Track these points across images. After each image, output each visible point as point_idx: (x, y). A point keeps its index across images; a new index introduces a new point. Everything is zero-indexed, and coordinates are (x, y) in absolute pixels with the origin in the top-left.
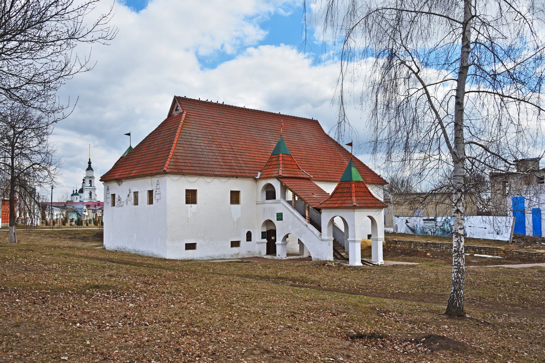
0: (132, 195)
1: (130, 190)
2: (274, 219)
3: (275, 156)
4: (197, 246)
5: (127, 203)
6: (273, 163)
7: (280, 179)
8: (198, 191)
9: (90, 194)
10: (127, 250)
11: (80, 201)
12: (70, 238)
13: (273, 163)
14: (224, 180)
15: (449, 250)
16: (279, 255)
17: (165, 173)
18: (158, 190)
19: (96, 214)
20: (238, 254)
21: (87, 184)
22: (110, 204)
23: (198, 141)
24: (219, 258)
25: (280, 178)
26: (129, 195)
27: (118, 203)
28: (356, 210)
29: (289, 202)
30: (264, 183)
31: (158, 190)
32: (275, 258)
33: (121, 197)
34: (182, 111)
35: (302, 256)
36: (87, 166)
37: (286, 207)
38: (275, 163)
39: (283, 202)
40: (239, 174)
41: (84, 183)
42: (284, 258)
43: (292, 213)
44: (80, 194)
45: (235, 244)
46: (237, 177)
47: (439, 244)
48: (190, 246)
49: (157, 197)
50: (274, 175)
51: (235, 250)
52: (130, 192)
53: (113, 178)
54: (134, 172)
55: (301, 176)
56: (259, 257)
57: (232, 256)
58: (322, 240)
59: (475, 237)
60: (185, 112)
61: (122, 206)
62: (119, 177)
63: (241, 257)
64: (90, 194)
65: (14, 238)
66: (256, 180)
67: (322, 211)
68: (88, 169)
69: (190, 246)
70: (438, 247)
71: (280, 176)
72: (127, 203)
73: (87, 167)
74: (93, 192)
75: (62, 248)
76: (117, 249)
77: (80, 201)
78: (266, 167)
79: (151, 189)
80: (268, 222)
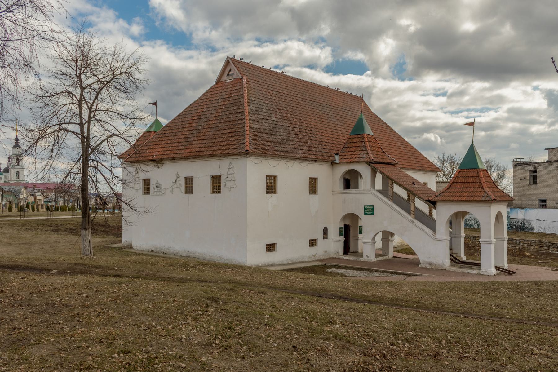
0: (182, 182)
1: (177, 174)
2: (360, 212)
3: (356, 136)
4: (278, 247)
5: (172, 191)
6: (355, 145)
7: (372, 164)
8: (278, 177)
9: (18, 173)
10: (172, 251)
11: (5, 182)
12: (53, 230)
13: (355, 145)
14: (303, 164)
15: (532, 247)
16: (367, 257)
17: (247, 153)
18: (229, 176)
19: (36, 197)
20: (315, 255)
21: (14, 161)
22: (141, 191)
23: (269, 115)
24: (299, 261)
25: (372, 163)
26: (176, 181)
27: (156, 190)
28: (493, 205)
29: (378, 191)
30: (344, 169)
31: (229, 176)
32: (362, 259)
33: (160, 182)
34: (240, 76)
35: (387, 257)
36: (14, 142)
37: (379, 198)
38: (358, 144)
39: (373, 191)
40: (319, 157)
41: (9, 161)
42: (373, 260)
43: (389, 205)
44: (4, 174)
45: (313, 243)
46: (315, 161)
47: (517, 240)
48: (271, 247)
49: (229, 184)
50: (361, 160)
51: (313, 251)
52: (178, 177)
53: (150, 158)
54: (187, 151)
55: (389, 161)
56: (336, 258)
57: (310, 258)
58: (437, 240)
59: (547, 232)
60: (245, 78)
61: (163, 194)
62: (159, 157)
63: (319, 259)
64: (18, 173)
65: (145, 257)
66: (333, 163)
67: (438, 204)
68: (14, 147)
69: (271, 247)
70: (516, 244)
71: (372, 161)
72: (172, 191)
73: (14, 144)
74: (21, 172)
75: (194, 266)
76: (153, 250)
77: (5, 182)
78: (345, 150)
79: (219, 174)
80: (353, 217)
